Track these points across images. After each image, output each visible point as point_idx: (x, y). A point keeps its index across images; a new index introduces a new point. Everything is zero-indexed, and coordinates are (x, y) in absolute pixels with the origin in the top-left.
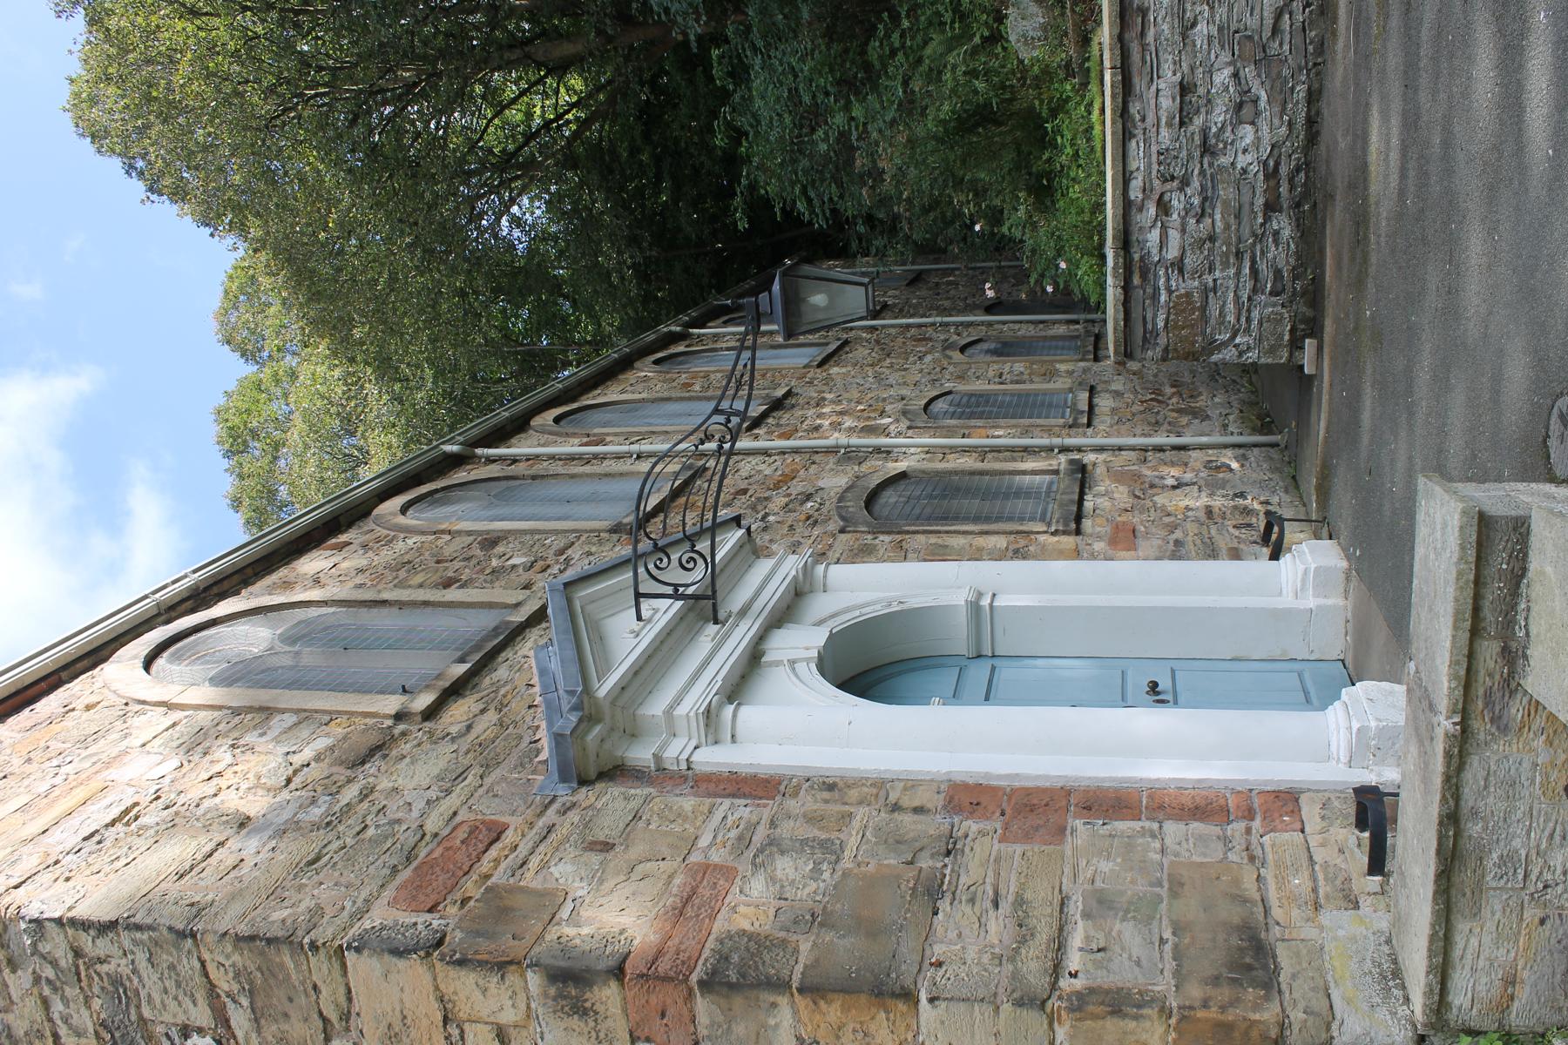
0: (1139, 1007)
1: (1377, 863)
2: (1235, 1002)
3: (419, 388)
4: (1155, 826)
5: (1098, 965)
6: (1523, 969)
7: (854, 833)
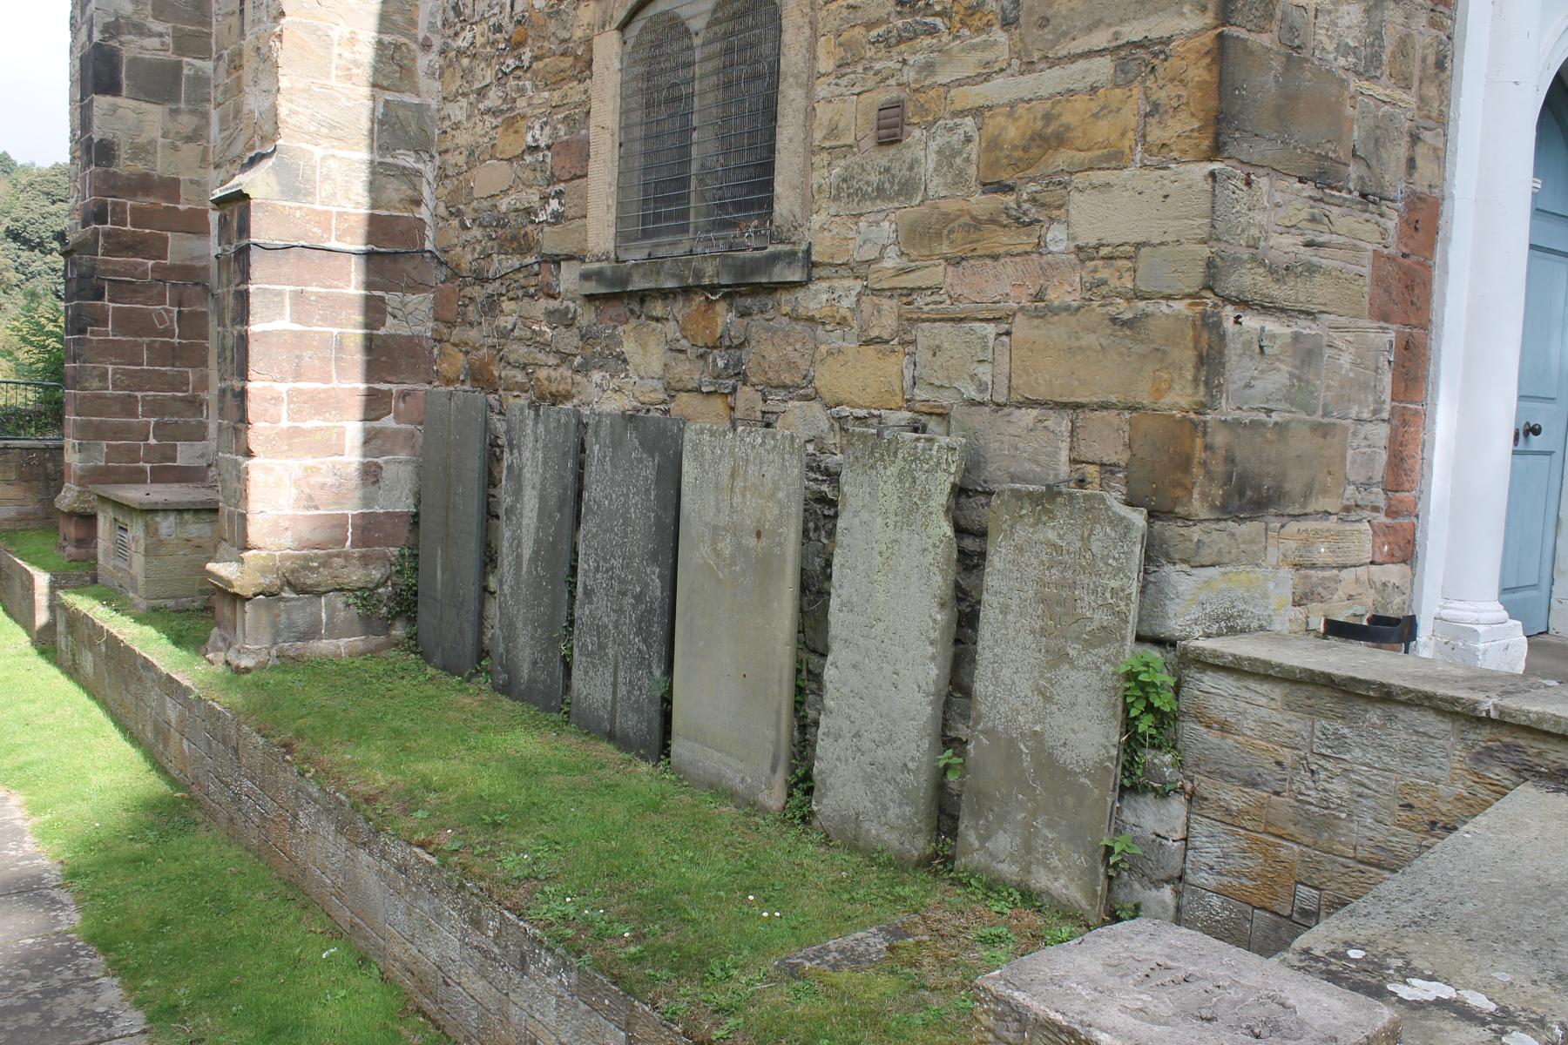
0: (1206, 383)
1: (1337, 630)
2: (1209, 475)
4: (1385, 415)
5: (1247, 345)
6: (1235, 741)
7: (1388, 92)
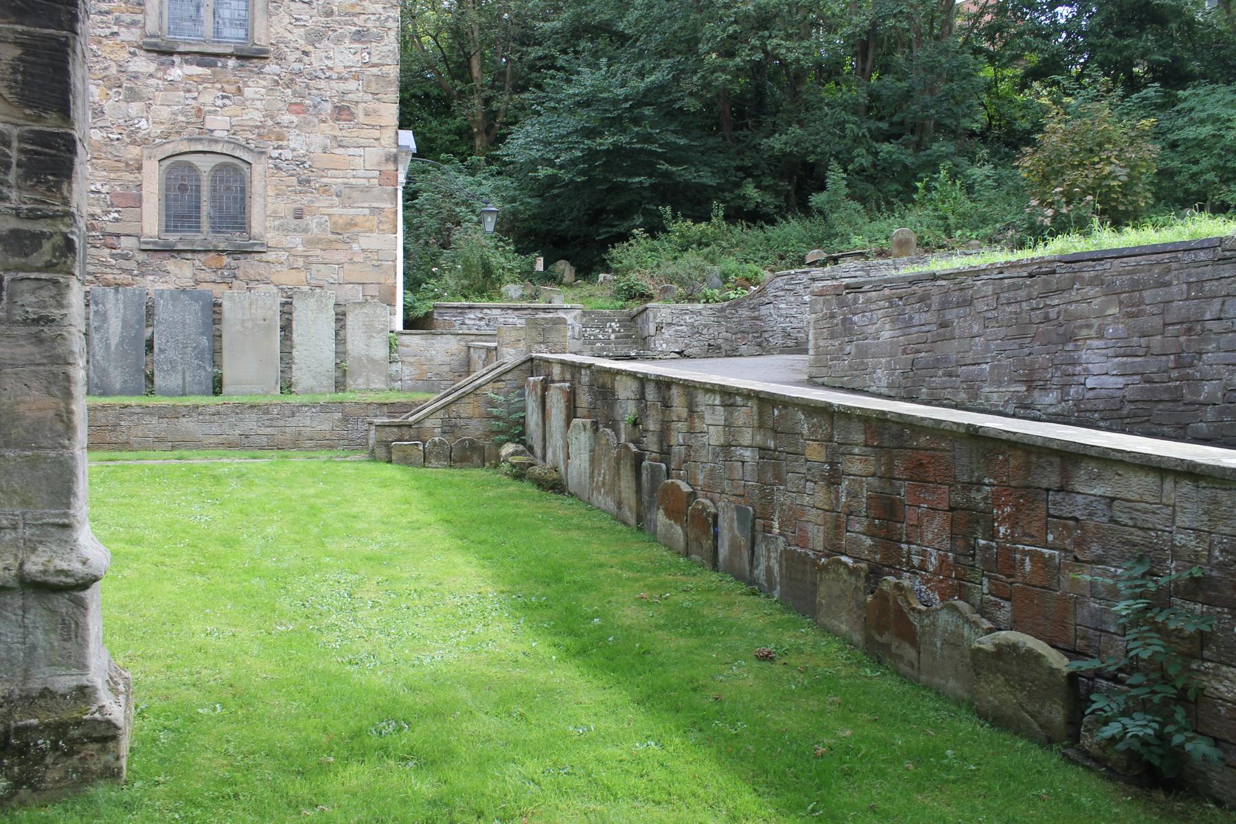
3: (939, 61)
